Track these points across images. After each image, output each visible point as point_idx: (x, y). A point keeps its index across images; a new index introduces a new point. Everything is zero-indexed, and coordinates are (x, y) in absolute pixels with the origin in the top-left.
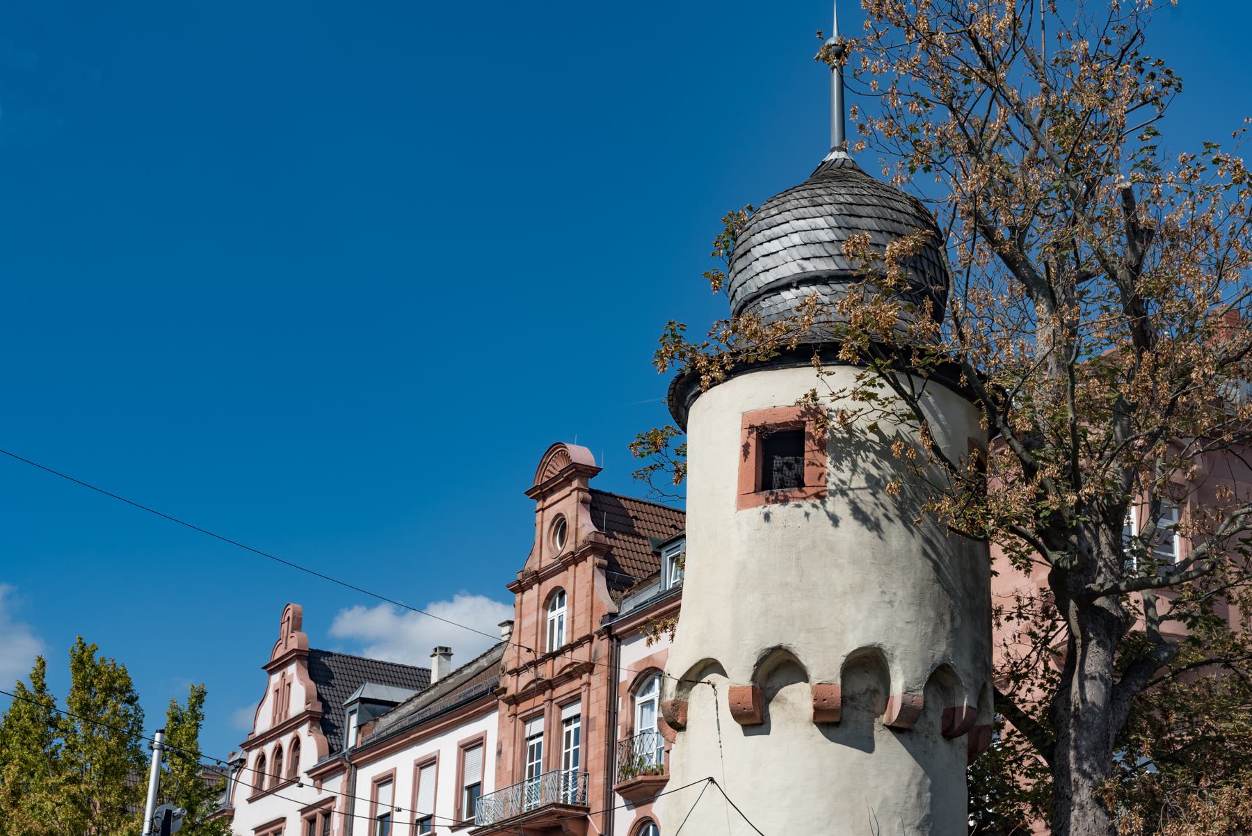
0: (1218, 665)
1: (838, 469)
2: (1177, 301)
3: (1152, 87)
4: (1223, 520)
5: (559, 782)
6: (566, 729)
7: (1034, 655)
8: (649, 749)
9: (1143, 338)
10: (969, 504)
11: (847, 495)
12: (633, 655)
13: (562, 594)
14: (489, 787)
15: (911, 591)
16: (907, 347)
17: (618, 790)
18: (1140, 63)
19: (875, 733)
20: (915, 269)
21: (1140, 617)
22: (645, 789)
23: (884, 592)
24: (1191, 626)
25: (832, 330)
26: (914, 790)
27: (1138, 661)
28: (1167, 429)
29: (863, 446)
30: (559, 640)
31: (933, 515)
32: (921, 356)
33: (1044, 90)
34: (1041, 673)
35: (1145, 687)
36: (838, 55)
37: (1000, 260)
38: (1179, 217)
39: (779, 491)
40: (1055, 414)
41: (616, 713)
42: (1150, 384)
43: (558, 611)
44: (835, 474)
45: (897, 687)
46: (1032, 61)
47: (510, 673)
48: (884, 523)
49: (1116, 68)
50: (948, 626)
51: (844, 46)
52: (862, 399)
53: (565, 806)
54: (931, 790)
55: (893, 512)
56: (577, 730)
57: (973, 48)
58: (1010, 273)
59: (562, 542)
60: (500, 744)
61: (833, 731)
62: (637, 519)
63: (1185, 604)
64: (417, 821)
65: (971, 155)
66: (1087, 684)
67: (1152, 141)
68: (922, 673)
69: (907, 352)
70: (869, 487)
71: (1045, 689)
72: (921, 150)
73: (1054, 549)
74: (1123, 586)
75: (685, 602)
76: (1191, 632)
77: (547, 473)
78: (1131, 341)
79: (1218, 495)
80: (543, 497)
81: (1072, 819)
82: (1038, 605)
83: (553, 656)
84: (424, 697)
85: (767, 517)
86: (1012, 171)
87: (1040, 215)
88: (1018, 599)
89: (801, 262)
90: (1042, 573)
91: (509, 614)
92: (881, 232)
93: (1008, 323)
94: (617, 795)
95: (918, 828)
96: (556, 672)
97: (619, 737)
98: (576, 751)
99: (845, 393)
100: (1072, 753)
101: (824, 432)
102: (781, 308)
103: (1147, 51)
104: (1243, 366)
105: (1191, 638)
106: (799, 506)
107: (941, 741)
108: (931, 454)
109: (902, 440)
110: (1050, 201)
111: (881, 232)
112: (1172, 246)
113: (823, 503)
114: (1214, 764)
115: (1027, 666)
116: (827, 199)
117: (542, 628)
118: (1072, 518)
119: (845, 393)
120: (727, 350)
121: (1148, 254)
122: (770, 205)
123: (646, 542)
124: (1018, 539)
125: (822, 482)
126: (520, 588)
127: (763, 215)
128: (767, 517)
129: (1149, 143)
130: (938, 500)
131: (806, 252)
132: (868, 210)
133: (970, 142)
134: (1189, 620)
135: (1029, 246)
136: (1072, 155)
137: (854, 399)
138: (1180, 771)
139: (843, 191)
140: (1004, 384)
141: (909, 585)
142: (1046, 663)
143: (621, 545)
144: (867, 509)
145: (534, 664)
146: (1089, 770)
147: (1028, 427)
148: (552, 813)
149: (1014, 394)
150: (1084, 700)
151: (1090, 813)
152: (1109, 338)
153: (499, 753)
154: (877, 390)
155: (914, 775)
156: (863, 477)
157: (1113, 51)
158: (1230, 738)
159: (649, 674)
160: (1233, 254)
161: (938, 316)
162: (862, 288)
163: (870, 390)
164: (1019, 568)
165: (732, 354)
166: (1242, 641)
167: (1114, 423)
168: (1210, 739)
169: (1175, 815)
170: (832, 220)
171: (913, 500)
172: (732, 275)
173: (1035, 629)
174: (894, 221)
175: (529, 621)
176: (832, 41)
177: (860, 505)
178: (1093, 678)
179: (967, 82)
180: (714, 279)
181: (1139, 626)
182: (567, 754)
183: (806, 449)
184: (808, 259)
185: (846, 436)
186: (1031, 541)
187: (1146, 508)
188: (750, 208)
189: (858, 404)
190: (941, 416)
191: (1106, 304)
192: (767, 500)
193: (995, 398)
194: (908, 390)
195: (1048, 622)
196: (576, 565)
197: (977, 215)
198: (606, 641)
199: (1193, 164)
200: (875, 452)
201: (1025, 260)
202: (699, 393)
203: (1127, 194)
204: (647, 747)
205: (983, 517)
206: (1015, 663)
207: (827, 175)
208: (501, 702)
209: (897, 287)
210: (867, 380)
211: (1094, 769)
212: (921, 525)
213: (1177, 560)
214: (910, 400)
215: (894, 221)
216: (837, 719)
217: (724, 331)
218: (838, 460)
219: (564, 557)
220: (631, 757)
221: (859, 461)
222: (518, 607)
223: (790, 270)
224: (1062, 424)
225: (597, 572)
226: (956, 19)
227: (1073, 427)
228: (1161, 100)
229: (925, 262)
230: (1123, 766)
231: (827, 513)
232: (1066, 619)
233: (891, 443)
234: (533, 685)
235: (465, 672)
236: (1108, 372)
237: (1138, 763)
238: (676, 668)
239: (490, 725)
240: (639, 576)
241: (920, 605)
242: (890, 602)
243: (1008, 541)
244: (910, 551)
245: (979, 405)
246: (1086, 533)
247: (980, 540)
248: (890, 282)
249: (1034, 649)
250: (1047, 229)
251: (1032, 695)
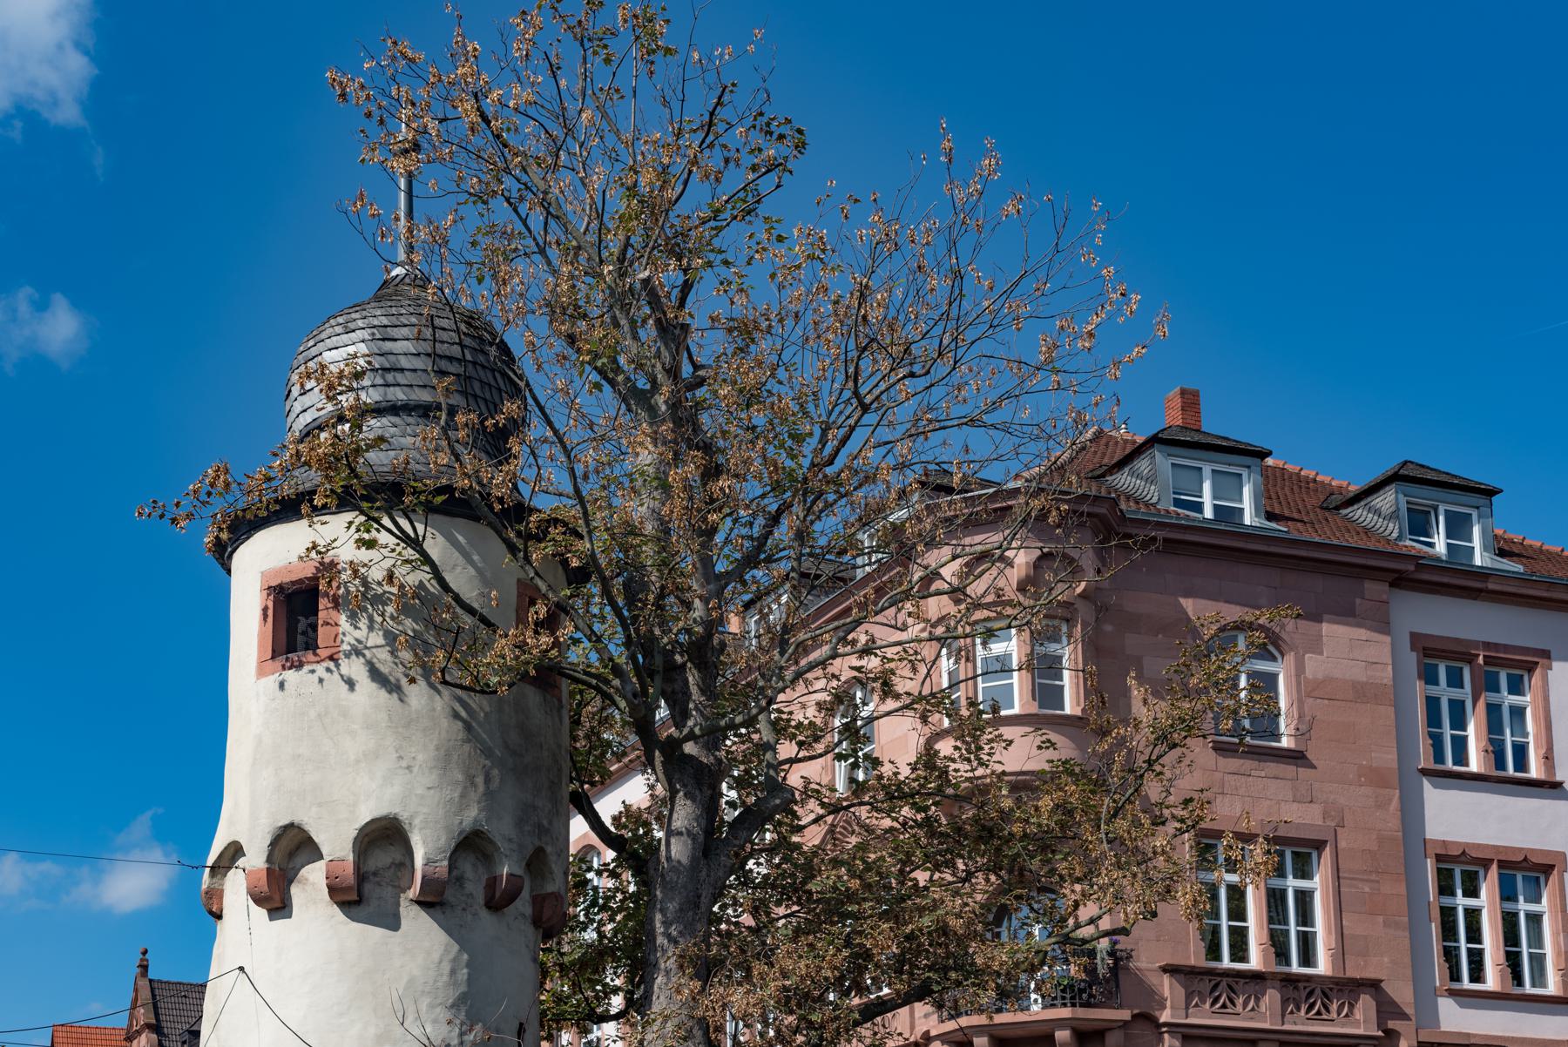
1: (356, 628)
23: (401, 758)
26: (446, 967)
50: (481, 788)
54: (468, 965)
61: (355, 910)
66: (673, 840)
85: (282, 685)
95: (452, 1006)
100: (658, 917)
106: (313, 671)
107: (484, 914)
113: (338, 666)
116: (360, 323)
128: (282, 685)
132: (405, 331)
141: (432, 747)
144: (384, 669)
150: (669, 858)
155: (446, 951)
178: (680, 834)
183: (321, 607)
190: (476, 558)
218: (353, 617)
242: (409, 768)
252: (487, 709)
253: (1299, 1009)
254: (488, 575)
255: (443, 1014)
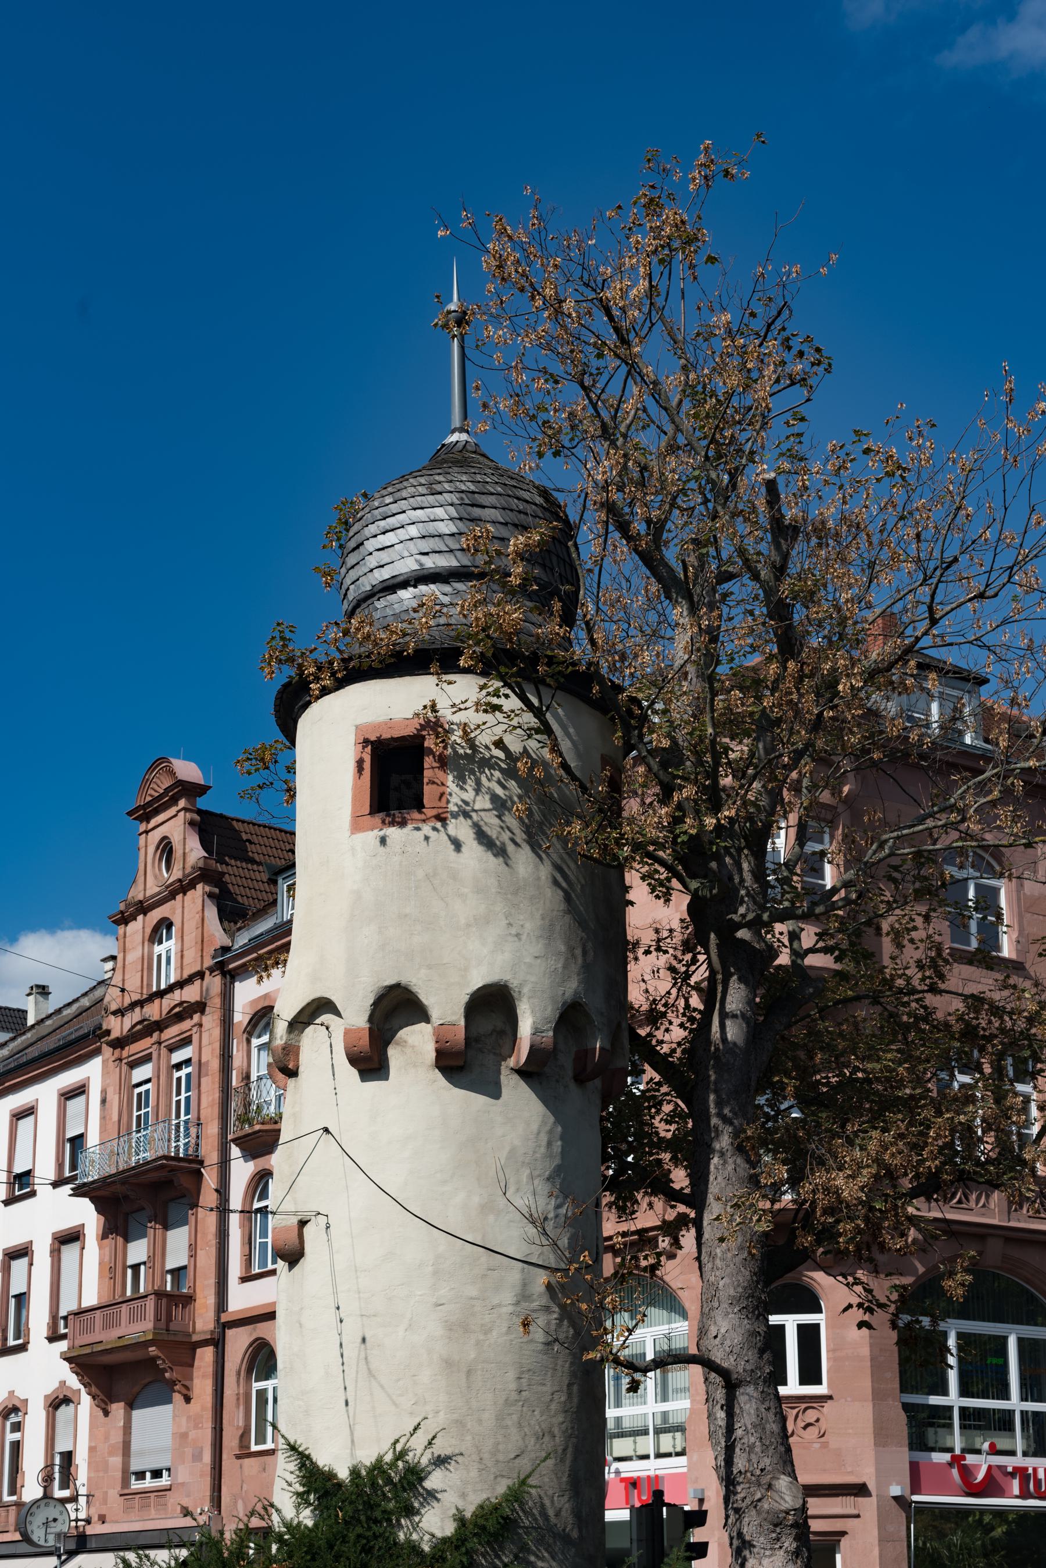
0: (867, 1001)
1: (462, 788)
2: (825, 606)
3: (800, 367)
4: (872, 844)
5: (169, 1132)
6: (176, 1075)
7: (674, 991)
8: (266, 1093)
9: (789, 644)
10: (601, 828)
11: (470, 817)
12: (247, 993)
13: (169, 926)
14: (93, 1139)
15: (539, 923)
16: (534, 653)
17: (233, 1140)
18: (788, 339)
19: (502, 1077)
20: (543, 566)
21: (784, 950)
22: (261, 1142)
23: (510, 924)
24: (837, 960)
25: (453, 634)
26: (544, 1138)
27: (783, 996)
28: (813, 745)
29: (487, 763)
30: (167, 976)
31: (564, 840)
32: (549, 664)
33: (684, 368)
34: (682, 1011)
35: (789, 1026)
36: (459, 323)
37: (637, 558)
38: (830, 512)
39: (396, 812)
40: (694, 729)
41: (230, 1057)
42: (795, 697)
43: (166, 945)
44: (457, 793)
45: (526, 1027)
46: (671, 334)
47: (114, 1013)
48: (510, 848)
49: (761, 345)
50: (580, 961)
51: (465, 313)
52: (485, 711)
53: (176, 1158)
54: (562, 1138)
55: (520, 836)
56: (188, 1076)
57: (605, 319)
58: (648, 573)
59: (168, 868)
60: (104, 1092)
62: (251, 842)
63: (832, 936)
64: (15, 1177)
65: (605, 439)
67: (799, 427)
68: (551, 1012)
69: (534, 659)
70: (494, 809)
71: (685, 1029)
72: (550, 432)
73: (693, 876)
74: (765, 917)
75: (294, 938)
76: (837, 967)
77: (151, 792)
78: (775, 650)
79: (866, 819)
80: (147, 818)
81: (712, 1167)
82: (678, 938)
83: (161, 994)
84: (20, 1040)
85: (383, 841)
86: (649, 457)
87: (679, 507)
88: (657, 931)
89: (419, 557)
90: (681, 901)
91: (111, 947)
92: (506, 524)
93: (645, 628)
94: (233, 1146)
95: (548, 1179)
96: (164, 1012)
97: (234, 1083)
98: (188, 1099)
99: (467, 705)
100: (712, 1097)
101: (445, 748)
102: (397, 608)
103: (797, 326)
104: (894, 678)
105: (837, 973)
106: (418, 829)
107: (572, 1085)
108: (562, 772)
109: (529, 756)
110: (689, 492)
111: (506, 524)
112: (820, 545)
113: (445, 826)
114: (861, 1106)
115: (666, 1005)
116: (447, 486)
117: (148, 964)
118: (711, 843)
119: (467, 705)
120: (338, 655)
121: (794, 553)
122: (384, 492)
123: (261, 868)
124: (657, 866)
125: (443, 804)
126: (123, 919)
127: (376, 504)
128: (383, 841)
129: (796, 430)
130: (568, 823)
131: (425, 545)
133: (604, 426)
134: (837, 953)
135: (666, 543)
136: (713, 440)
137: (477, 711)
138: (824, 1115)
139: (464, 478)
140: (640, 696)
141: (538, 916)
142: (687, 1000)
143: (233, 871)
144: (493, 833)
145: (140, 1003)
146: (729, 1115)
147: (665, 743)
148: (162, 1166)
149: (650, 707)
150: (724, 1038)
151: (730, 1161)
152: (751, 646)
153: (104, 1101)
154: (502, 701)
155: (544, 1122)
156: (487, 797)
157: (758, 325)
158: (878, 1080)
159: (263, 1017)
160: (885, 555)
161: (568, 619)
162: (484, 587)
163: (495, 701)
164: (658, 897)
165: (343, 660)
166: (891, 975)
167: (757, 739)
168: (857, 1079)
169: (822, 1162)
170: (452, 510)
171: (541, 823)
172: (343, 571)
173: (675, 963)
174: (520, 512)
175: (134, 956)
176: (452, 307)
177: (485, 828)
178: (735, 1016)
179: (600, 356)
180: (325, 574)
181: (784, 959)
182: (178, 1102)
183: (426, 765)
184: (427, 554)
185: (469, 751)
186: (669, 868)
187: (793, 832)
188: (365, 495)
189: (482, 717)
190: (571, 730)
191: (749, 607)
192: (383, 822)
193: (630, 712)
194: (535, 701)
195: (688, 957)
196: (185, 894)
197: (610, 507)
198: (219, 978)
199: (842, 453)
200: (501, 770)
201: (662, 558)
202: (309, 703)
203: (771, 486)
204: (264, 1094)
205: (617, 842)
206: (654, 1000)
207: (450, 459)
208: (104, 1046)
209: (523, 586)
210: (491, 689)
211: (735, 1114)
212: (551, 850)
213: (828, 887)
214: (538, 713)
215: (520, 512)
216: (461, 1063)
217: (333, 633)
218: (461, 779)
219: (171, 885)
220: (247, 1104)
221: (484, 779)
222: (121, 940)
223: (407, 566)
224: (701, 740)
225: (208, 901)
226: (587, 285)
227: (713, 742)
228: (810, 382)
229: (554, 559)
230: (766, 1109)
231: (449, 836)
232: (707, 953)
233: (517, 759)
234: (139, 1027)
235: (65, 1013)
236: (751, 683)
237: (783, 1107)
238: (286, 1009)
239: (92, 1071)
240: (255, 906)
241: (549, 938)
242: (518, 935)
243: (647, 868)
244: (539, 879)
245: (613, 719)
246: (727, 859)
247: (614, 867)
248: (515, 581)
249: (674, 985)
250: (686, 524)
251: (673, 1035)
252: (583, 882)
253: (1021, 1208)
254: (581, 747)
255: (542, 1187)
